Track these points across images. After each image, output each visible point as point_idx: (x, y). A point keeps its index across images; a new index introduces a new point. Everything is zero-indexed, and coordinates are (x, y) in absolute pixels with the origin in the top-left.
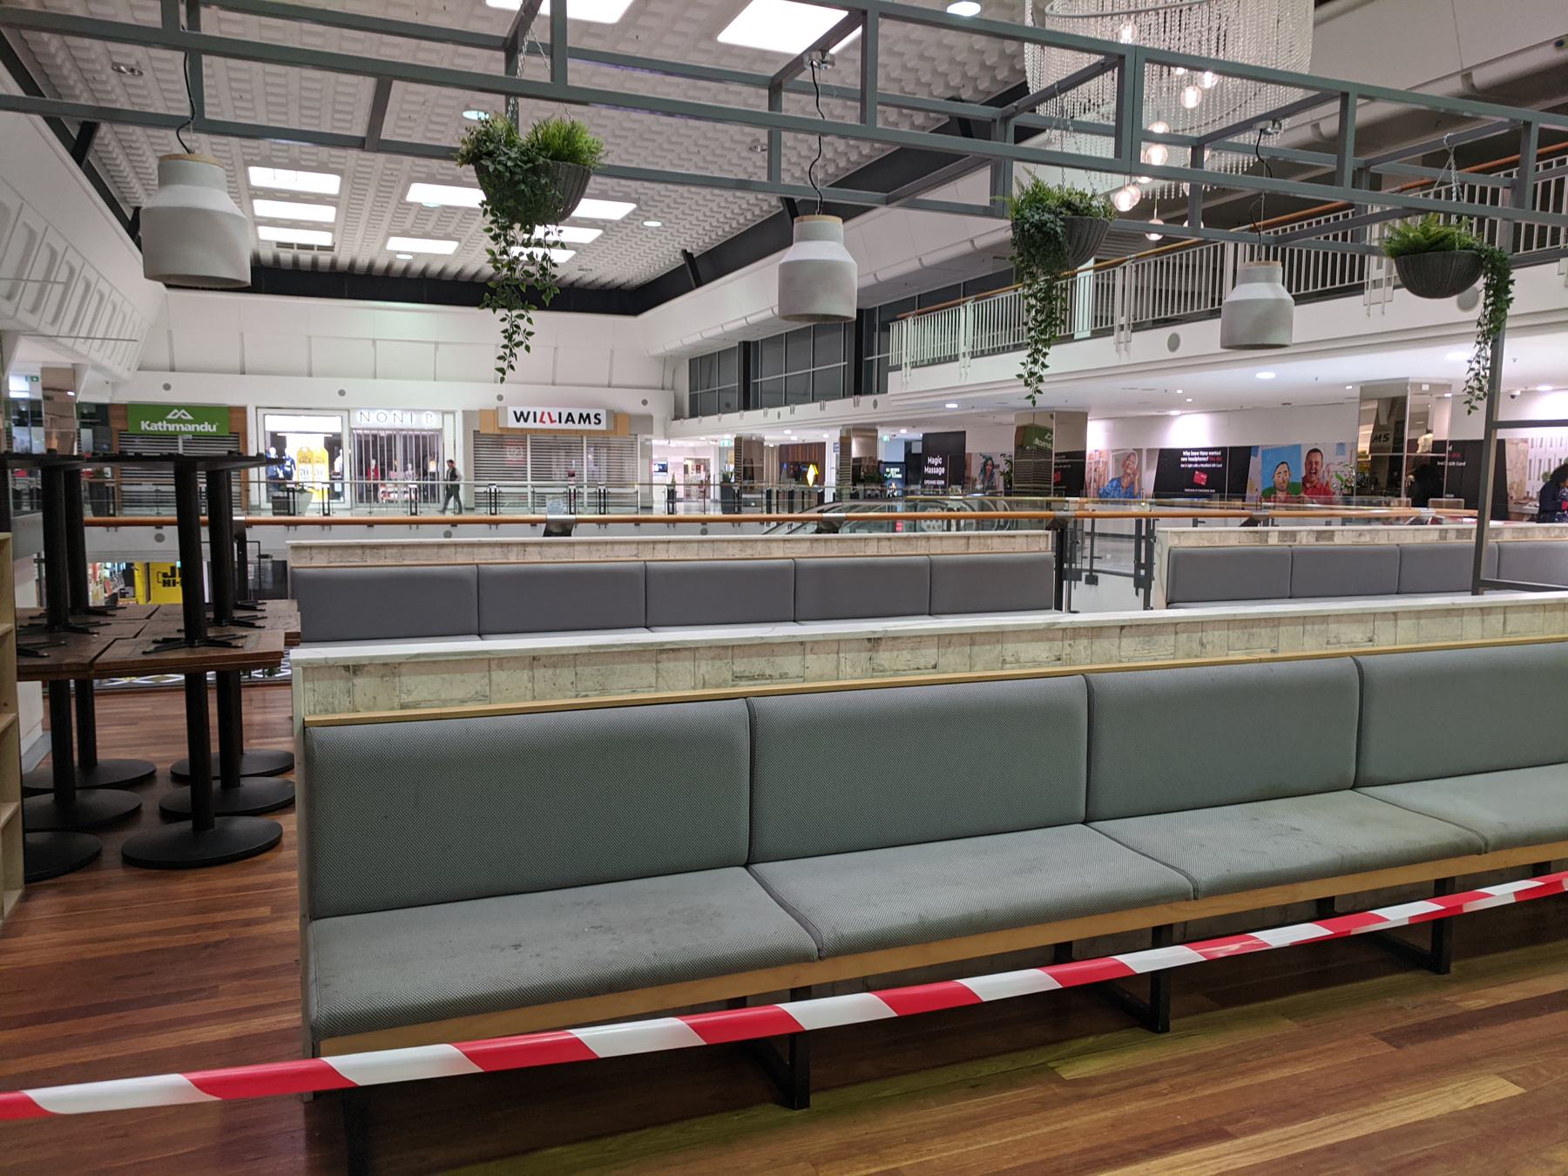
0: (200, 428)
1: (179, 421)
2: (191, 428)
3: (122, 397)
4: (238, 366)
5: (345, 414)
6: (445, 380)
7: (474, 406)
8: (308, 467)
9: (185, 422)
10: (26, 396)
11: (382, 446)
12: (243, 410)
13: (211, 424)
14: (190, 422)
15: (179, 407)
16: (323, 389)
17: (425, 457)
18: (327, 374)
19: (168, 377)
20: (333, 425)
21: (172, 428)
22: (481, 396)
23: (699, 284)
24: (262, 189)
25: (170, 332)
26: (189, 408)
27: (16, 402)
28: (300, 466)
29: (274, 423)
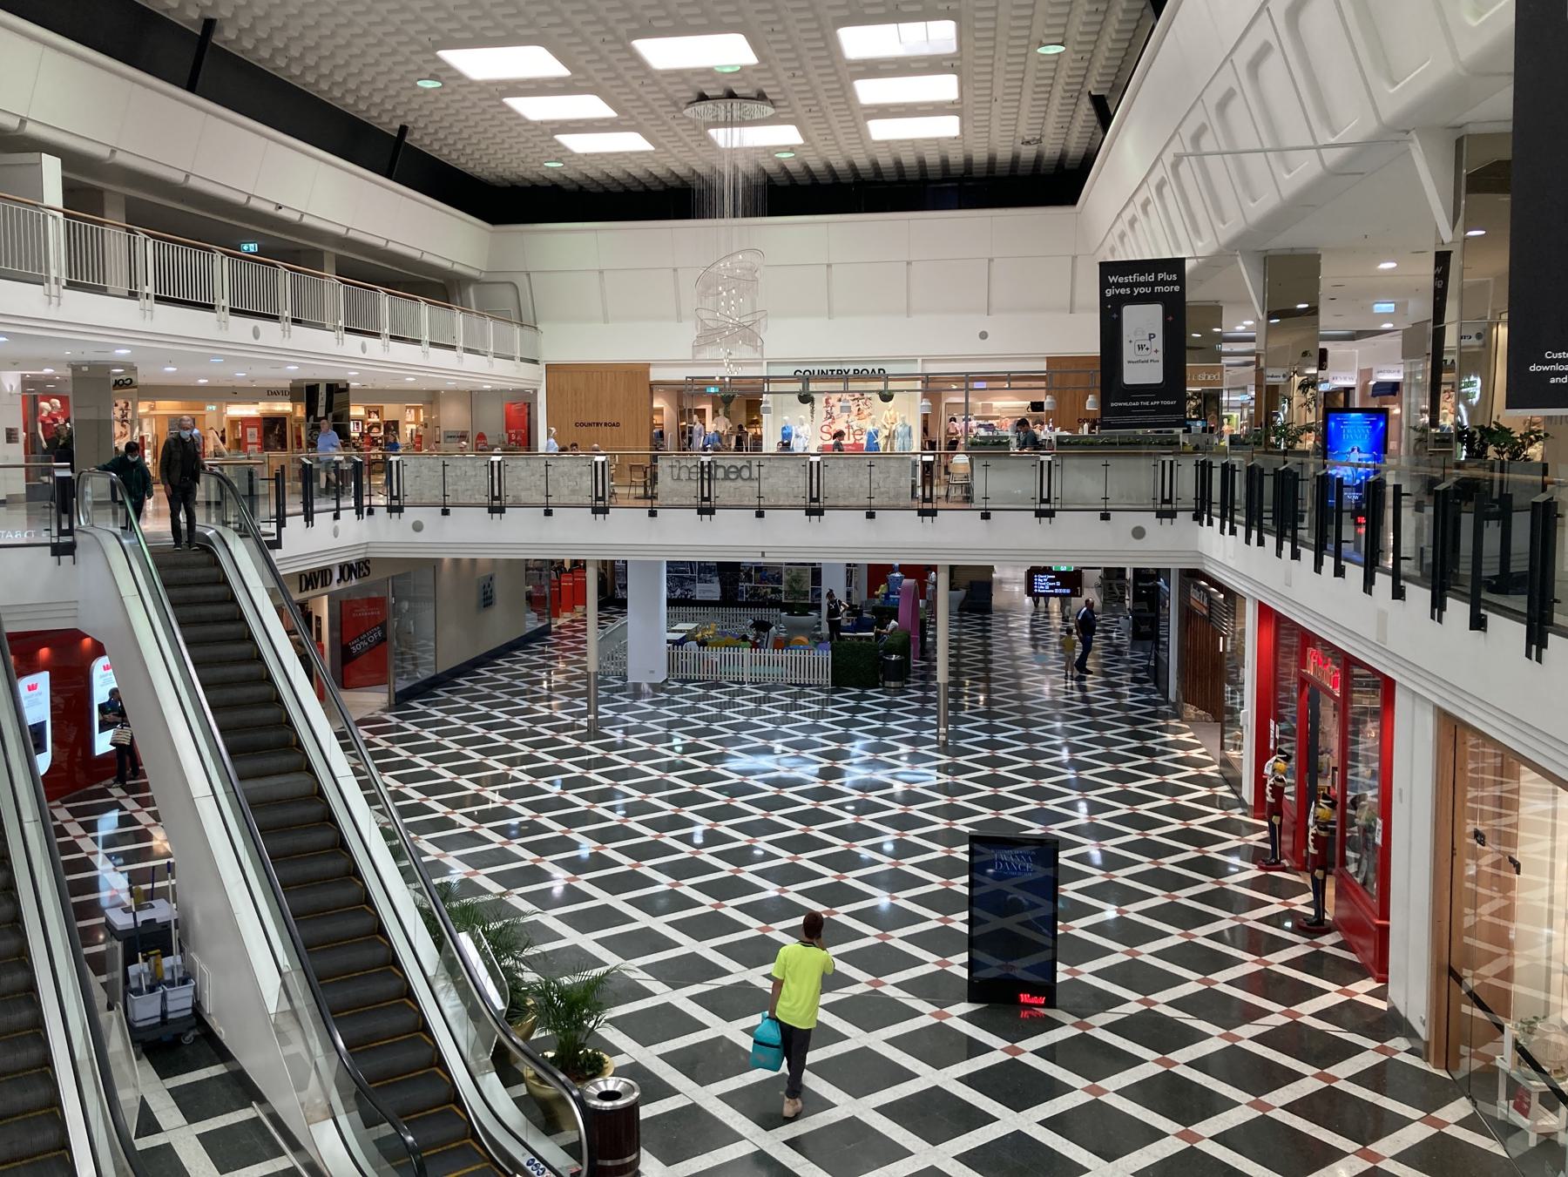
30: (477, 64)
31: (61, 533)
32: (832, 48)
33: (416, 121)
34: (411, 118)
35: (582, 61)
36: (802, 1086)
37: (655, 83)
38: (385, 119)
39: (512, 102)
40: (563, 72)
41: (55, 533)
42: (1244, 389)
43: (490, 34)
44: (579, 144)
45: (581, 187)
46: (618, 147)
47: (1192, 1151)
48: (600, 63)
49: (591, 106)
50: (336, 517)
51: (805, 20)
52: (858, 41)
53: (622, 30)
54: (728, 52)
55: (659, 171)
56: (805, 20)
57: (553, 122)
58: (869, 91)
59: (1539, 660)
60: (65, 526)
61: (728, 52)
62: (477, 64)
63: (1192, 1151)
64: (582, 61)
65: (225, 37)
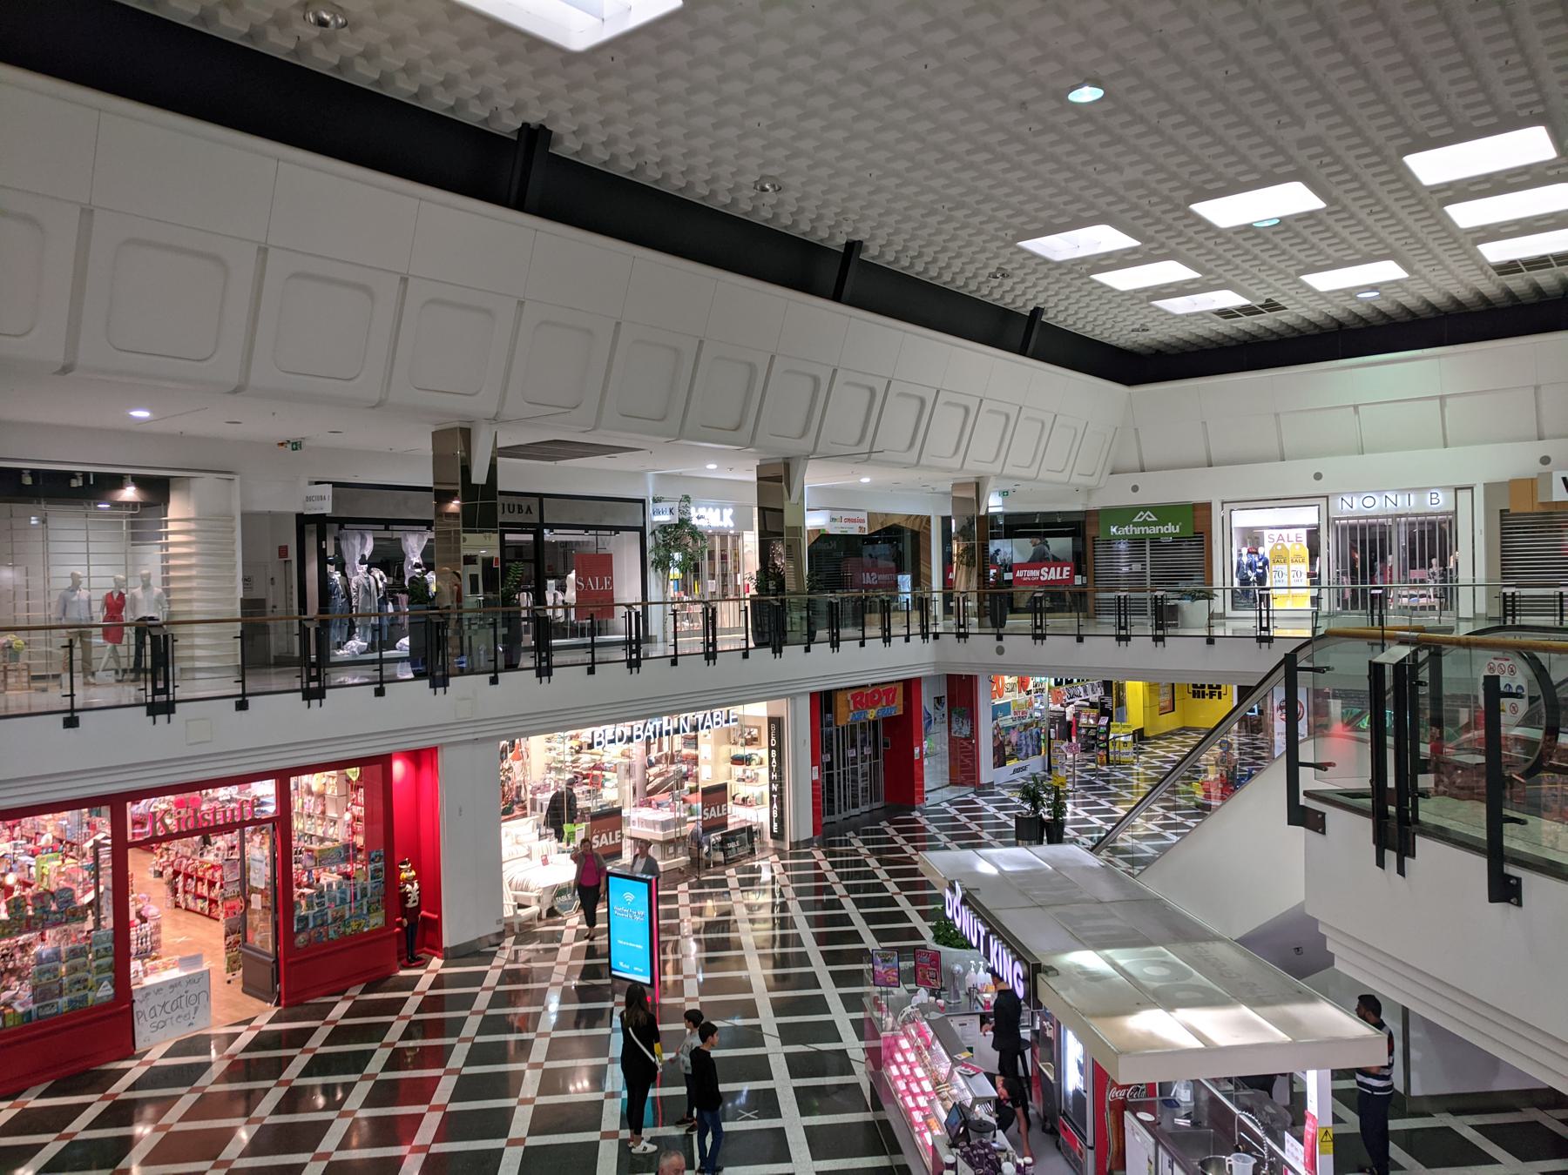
0: (1163, 530)
1: (1145, 523)
2: (1155, 530)
3: (1096, 504)
4: (1137, 465)
5: (1323, 502)
6: (1456, 445)
7: (1503, 475)
8: (1283, 568)
9: (1149, 524)
10: (1000, 510)
11: (1373, 542)
12: (1207, 506)
13: (1175, 524)
14: (1154, 524)
15: (1145, 509)
16: (1295, 476)
17: (324, 626)
18: (1302, 455)
19: (1136, 479)
20: (1309, 516)
21: (1137, 531)
22: (1510, 461)
23: (1022, 352)
24: (1450, 185)
25: (1204, 423)
26: (1155, 509)
27: (994, 516)
28: (1273, 567)
29: (1243, 519)
30: (1059, 246)
31: (156, 692)
32: (1407, 180)
33: (1046, 302)
34: (1040, 300)
35: (1150, 231)
36: (1388, 1158)
37: (1229, 241)
38: (1019, 303)
39: (1100, 277)
40: (1133, 243)
41: (150, 692)
42: (182, 670)
43: (1209, 187)
44: (1178, 305)
45: (1254, 337)
46: (1206, 306)
47: (428, 1102)
48: (1165, 230)
49: (1171, 271)
50: (862, 645)
51: (1365, 156)
52: (1432, 166)
53: (1180, 195)
54: (1294, 198)
55: (1409, 301)
56: (1365, 156)
57: (1145, 290)
58: (1465, 215)
59: (1401, 871)
60: (160, 685)
61: (1294, 198)
62: (1059, 246)
63: (428, 1102)
64: (1150, 231)
65: (871, 253)
